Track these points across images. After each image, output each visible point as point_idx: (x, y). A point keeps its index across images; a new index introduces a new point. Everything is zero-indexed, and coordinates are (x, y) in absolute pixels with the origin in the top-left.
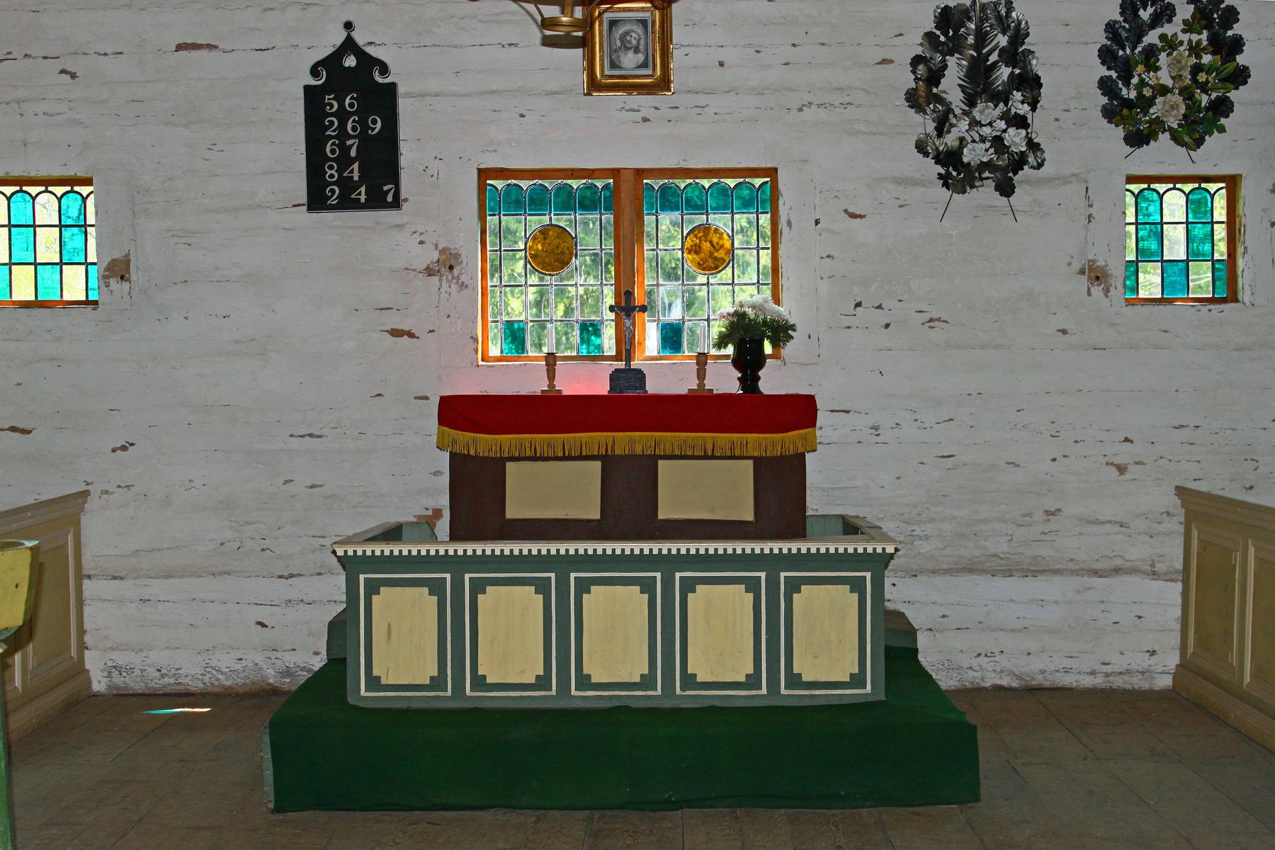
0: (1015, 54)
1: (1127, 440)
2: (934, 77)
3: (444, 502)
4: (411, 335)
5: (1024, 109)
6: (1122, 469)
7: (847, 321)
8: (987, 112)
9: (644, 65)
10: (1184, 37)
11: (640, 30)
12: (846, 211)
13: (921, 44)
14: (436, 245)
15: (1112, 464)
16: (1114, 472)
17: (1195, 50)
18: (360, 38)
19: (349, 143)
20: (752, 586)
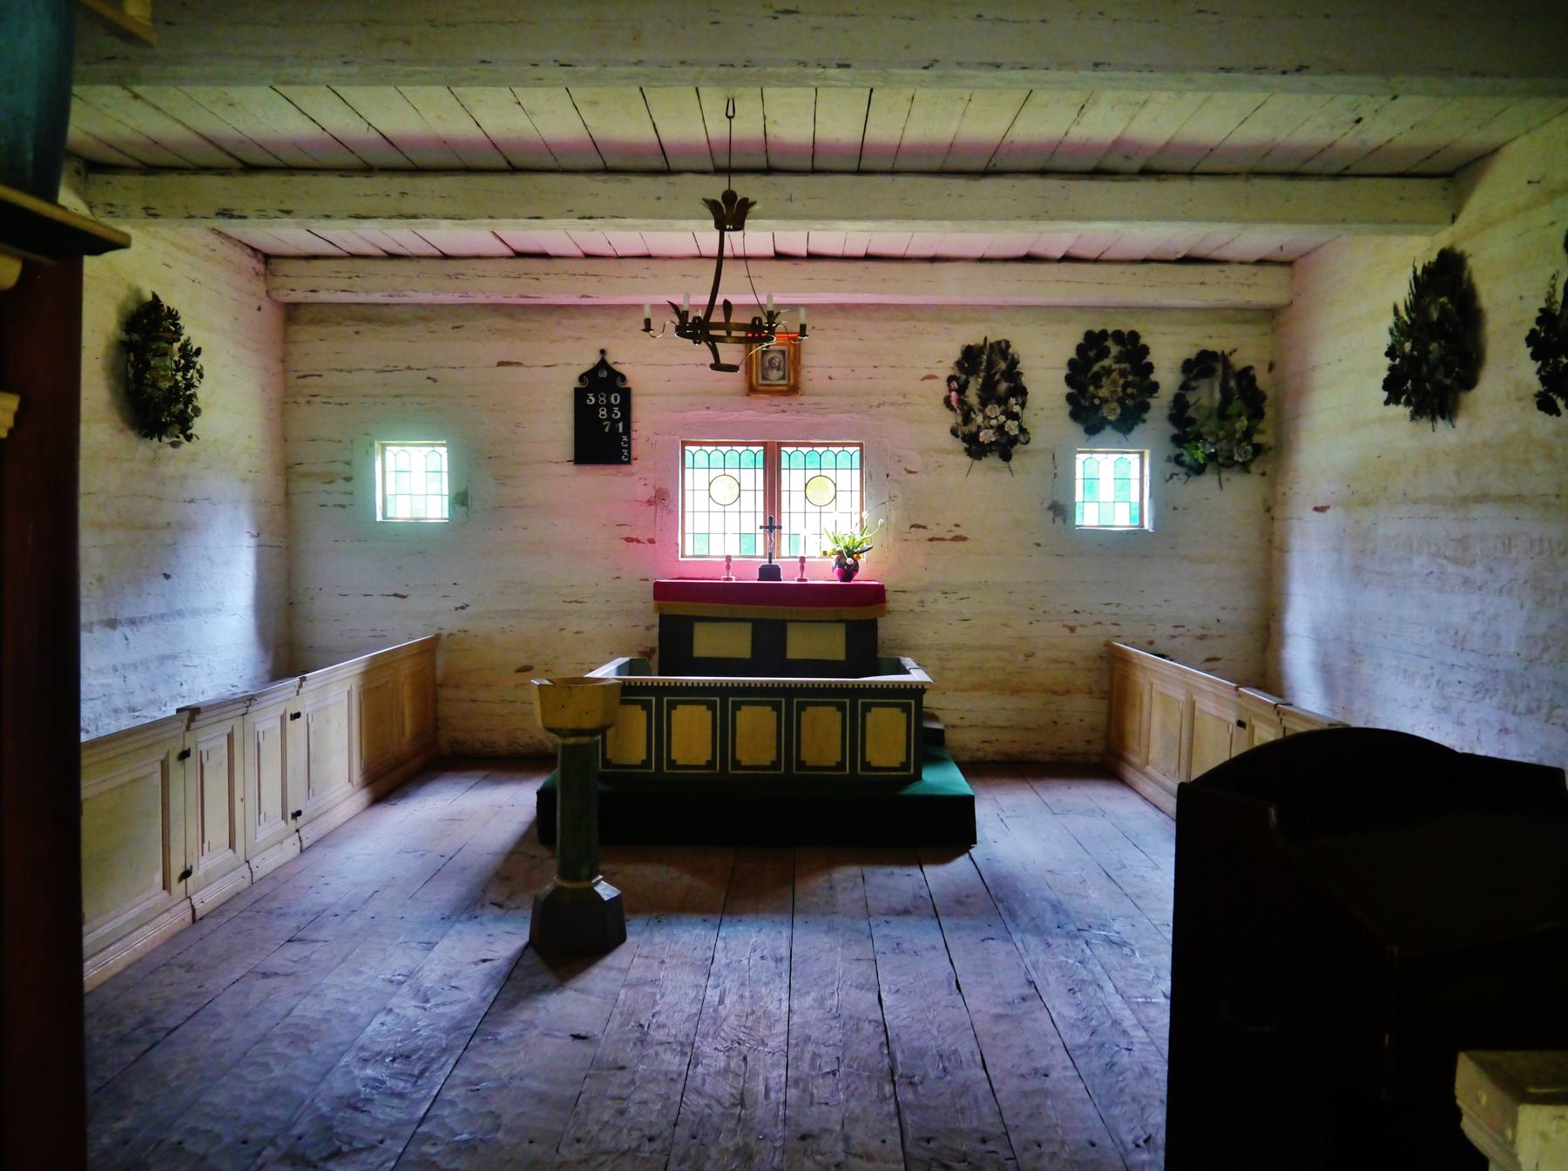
0: (1013, 374)
1: (1076, 612)
2: (962, 390)
3: (656, 644)
5: (1017, 409)
6: (1072, 629)
7: (905, 536)
8: (994, 410)
9: (783, 378)
10: (1115, 366)
11: (780, 356)
12: (905, 469)
13: (953, 368)
14: (654, 487)
15: (1066, 626)
16: (1067, 631)
17: (1123, 373)
18: (610, 359)
20: (841, 707)
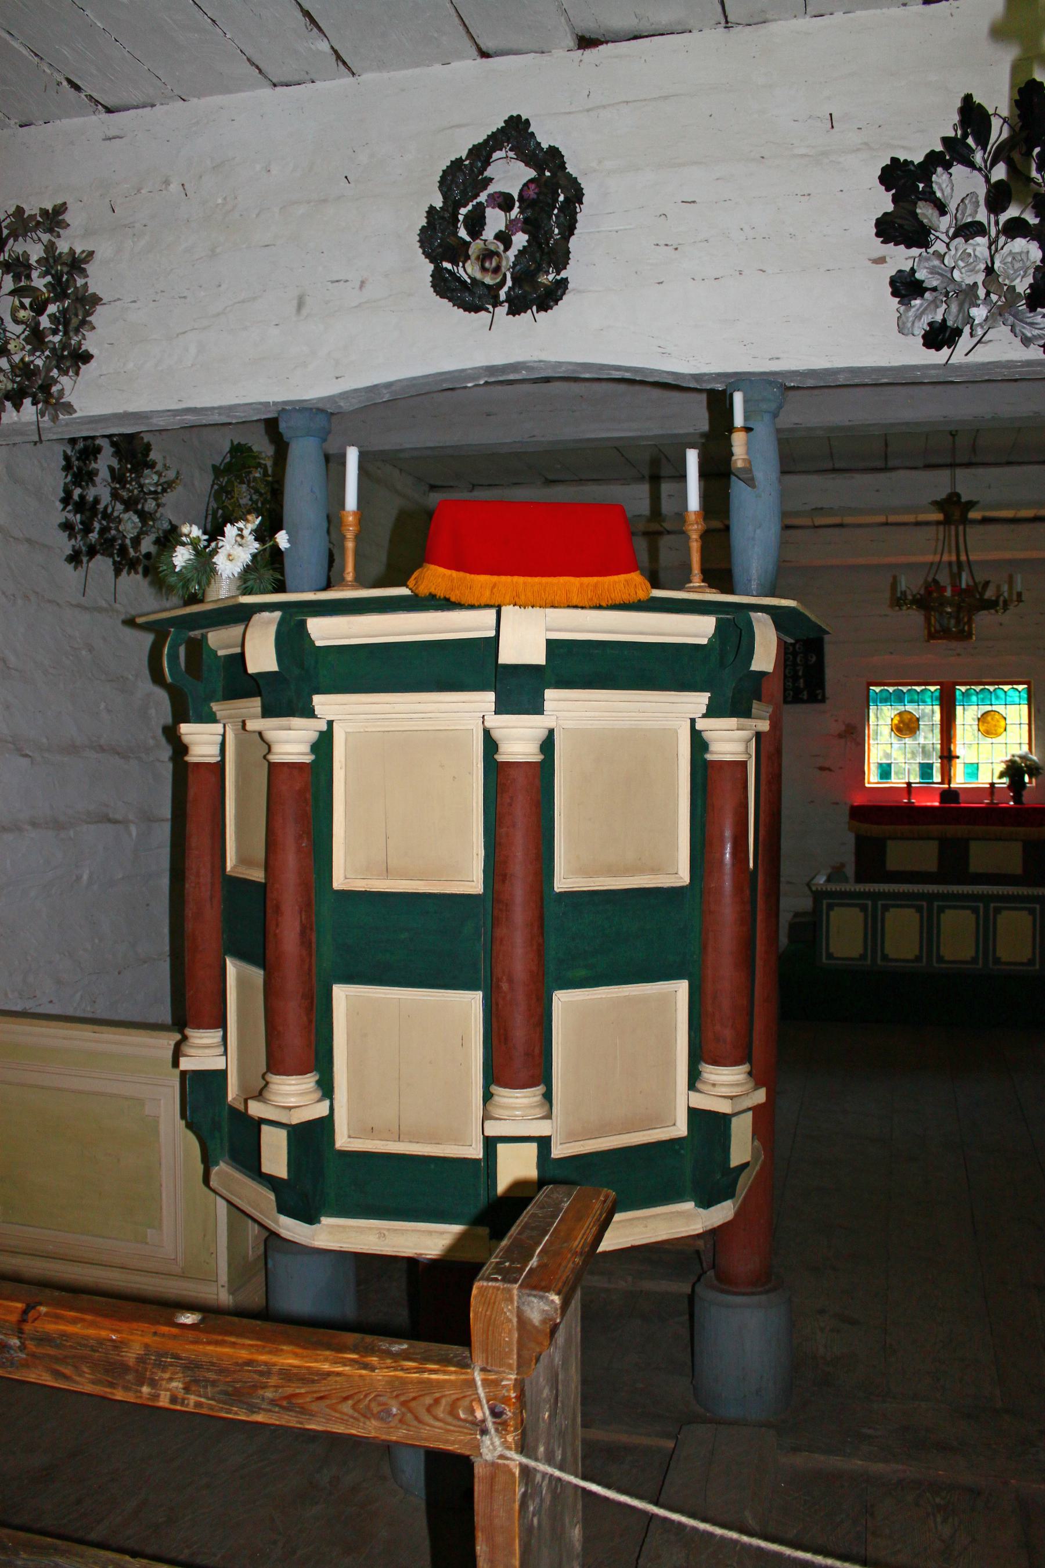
4: (830, 770)
19: (798, 668)
